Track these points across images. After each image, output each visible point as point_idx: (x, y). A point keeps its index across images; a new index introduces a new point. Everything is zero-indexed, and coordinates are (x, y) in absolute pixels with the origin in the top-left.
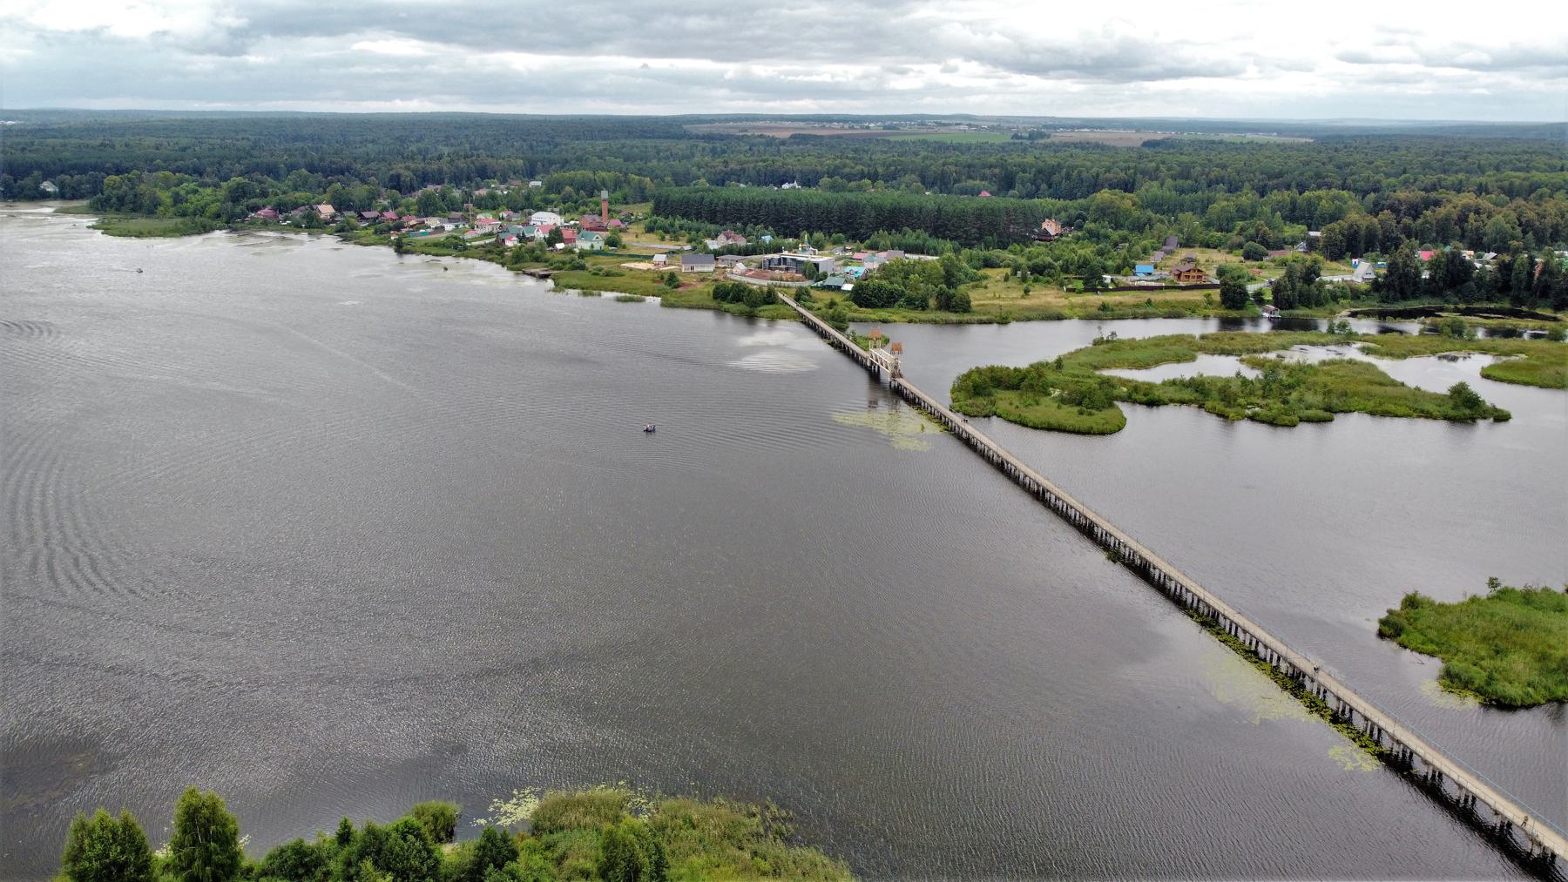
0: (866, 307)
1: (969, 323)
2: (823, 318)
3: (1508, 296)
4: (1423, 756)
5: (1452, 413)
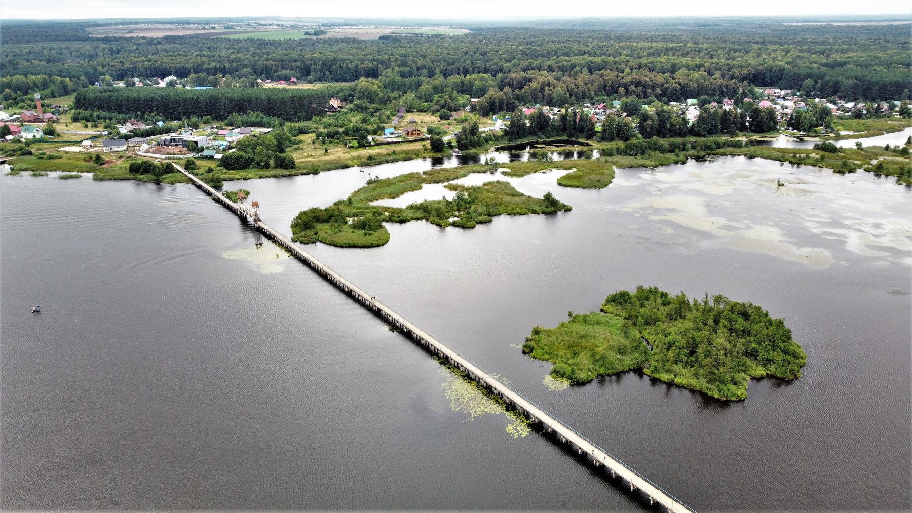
5: (546, 210)
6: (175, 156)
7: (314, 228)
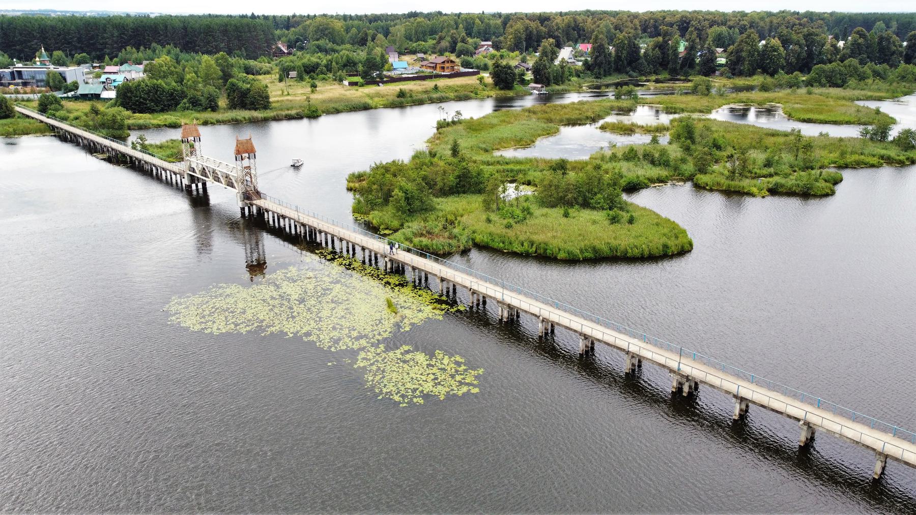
0: (140, 112)
1: (266, 120)
2: (87, 127)
6: (19, 96)
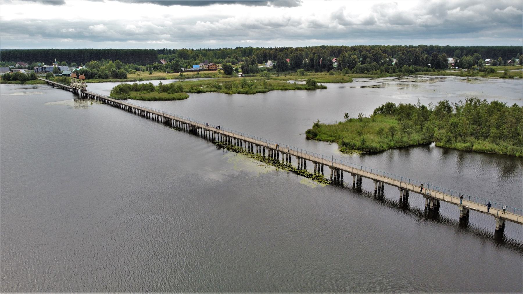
3: (314, 69)
4: (352, 171)
5: (308, 87)
7: (129, 93)
